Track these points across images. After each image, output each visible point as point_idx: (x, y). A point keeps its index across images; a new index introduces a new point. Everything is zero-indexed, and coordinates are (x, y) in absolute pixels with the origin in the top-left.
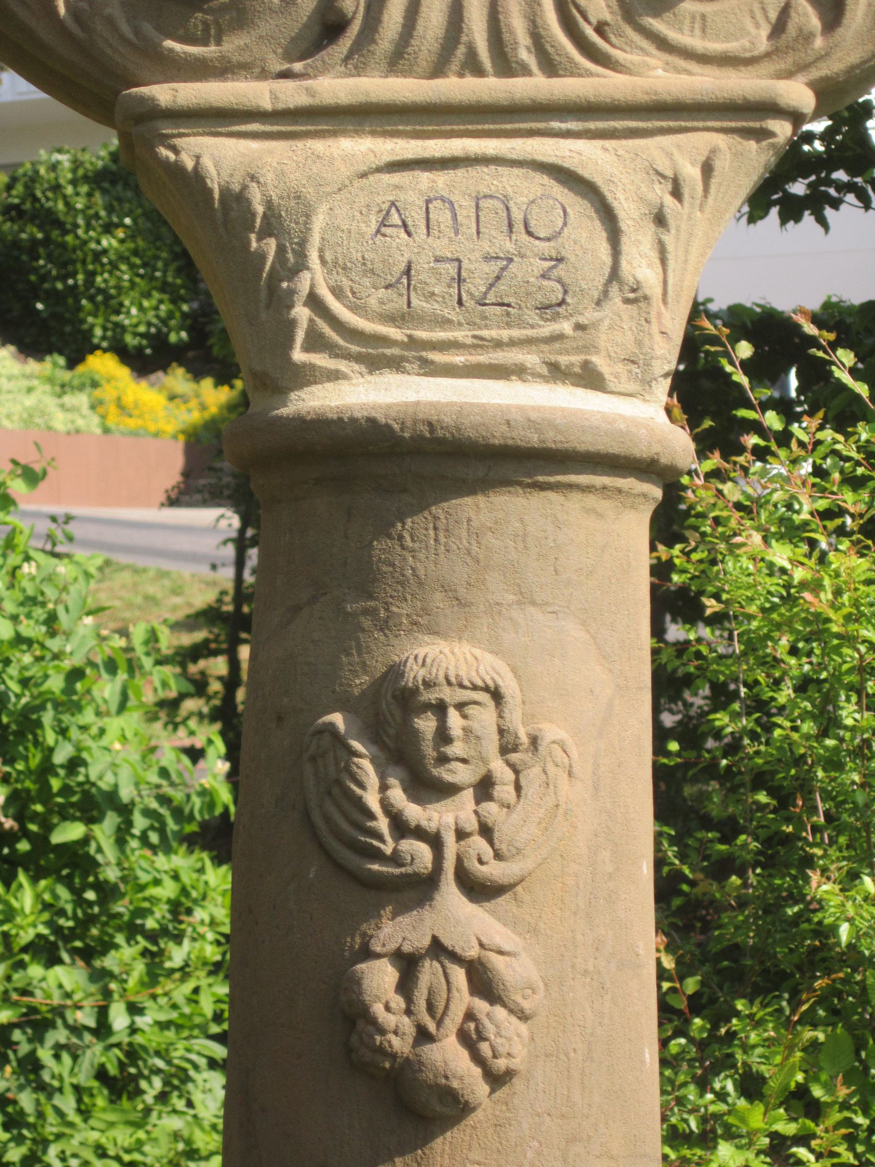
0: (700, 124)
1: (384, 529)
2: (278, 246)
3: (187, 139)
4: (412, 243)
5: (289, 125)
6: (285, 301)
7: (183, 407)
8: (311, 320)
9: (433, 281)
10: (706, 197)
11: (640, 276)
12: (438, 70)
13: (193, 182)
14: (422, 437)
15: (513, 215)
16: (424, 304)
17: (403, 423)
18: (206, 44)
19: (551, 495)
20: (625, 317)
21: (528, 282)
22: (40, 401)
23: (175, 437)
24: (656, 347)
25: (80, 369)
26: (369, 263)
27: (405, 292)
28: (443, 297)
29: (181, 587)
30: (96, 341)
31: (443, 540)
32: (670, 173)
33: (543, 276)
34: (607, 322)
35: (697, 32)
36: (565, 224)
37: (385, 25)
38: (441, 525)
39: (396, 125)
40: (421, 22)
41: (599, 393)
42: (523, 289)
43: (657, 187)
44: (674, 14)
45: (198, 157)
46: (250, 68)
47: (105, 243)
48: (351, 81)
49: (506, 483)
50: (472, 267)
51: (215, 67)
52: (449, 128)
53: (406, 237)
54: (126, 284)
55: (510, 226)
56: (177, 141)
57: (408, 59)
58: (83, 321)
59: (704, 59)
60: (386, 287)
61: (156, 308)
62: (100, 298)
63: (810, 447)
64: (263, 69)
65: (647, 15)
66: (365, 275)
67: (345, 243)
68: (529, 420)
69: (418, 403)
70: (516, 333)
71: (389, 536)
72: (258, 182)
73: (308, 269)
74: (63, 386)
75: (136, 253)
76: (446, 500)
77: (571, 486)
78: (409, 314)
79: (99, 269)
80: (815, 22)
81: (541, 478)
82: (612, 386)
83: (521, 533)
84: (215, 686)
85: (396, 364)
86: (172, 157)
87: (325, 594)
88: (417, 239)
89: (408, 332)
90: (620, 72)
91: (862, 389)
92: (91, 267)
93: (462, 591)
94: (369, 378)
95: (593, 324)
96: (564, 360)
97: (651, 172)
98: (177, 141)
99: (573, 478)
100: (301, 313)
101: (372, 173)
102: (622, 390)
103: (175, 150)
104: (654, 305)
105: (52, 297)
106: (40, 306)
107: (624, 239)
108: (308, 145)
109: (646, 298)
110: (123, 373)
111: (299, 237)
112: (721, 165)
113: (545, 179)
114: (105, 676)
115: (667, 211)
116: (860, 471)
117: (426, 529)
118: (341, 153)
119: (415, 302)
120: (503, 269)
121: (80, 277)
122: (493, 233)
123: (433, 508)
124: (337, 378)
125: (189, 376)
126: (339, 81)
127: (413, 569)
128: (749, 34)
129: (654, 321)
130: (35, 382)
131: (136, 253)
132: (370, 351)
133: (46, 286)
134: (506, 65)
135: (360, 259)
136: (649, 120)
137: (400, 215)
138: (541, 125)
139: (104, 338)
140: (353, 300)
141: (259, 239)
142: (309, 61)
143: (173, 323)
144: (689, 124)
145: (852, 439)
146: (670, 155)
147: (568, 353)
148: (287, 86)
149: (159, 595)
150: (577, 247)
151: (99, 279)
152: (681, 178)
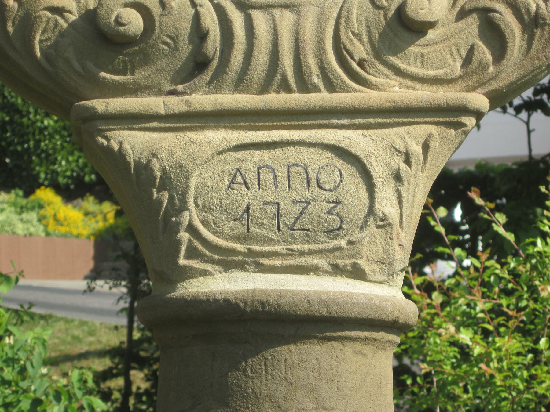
0: (422, 120)
1: (235, 365)
2: (169, 196)
3: (114, 132)
4: (249, 194)
5: (176, 123)
6: (175, 228)
7: (93, 220)
8: (190, 240)
9: (263, 216)
10: (425, 163)
11: (386, 212)
12: (264, 90)
13: (119, 157)
14: (257, 311)
15: (310, 176)
16: (257, 230)
17: (246, 303)
18: (125, 75)
19: (335, 344)
20: (377, 236)
21: (319, 216)
22: (8, 217)
23: (88, 237)
24: (396, 254)
25: (32, 197)
26: (224, 206)
27: (246, 223)
28: (269, 226)
29: (94, 331)
30: (41, 181)
31: (270, 371)
32: (403, 150)
33: (328, 213)
34: (367, 240)
35: (419, 64)
36: (341, 181)
37: (232, 63)
38: (269, 363)
39: (239, 123)
40: (254, 61)
41: (362, 282)
42: (316, 220)
43: (396, 158)
44: (405, 53)
45: (121, 143)
46: (151, 89)
47: (46, 123)
48: (212, 97)
49: (307, 337)
50: (286, 207)
51: (130, 88)
52: (271, 124)
53: (246, 190)
54: (59, 147)
55: (308, 183)
56: (109, 133)
57: (246, 83)
58: (34, 169)
59: (423, 80)
60: (235, 220)
61: (77, 161)
62: (43, 155)
63: (481, 270)
64: (159, 89)
65: (389, 55)
66: (221, 213)
67: (210, 194)
68: (321, 300)
69: (254, 290)
70: (312, 247)
71: (238, 370)
72: (157, 158)
73: (188, 209)
74: (22, 208)
75: (64, 128)
76: (272, 348)
77: (346, 338)
78: (248, 236)
79: (42, 138)
80: (489, 57)
81: (328, 334)
82: (370, 278)
83: (317, 367)
84: (116, 395)
85: (241, 266)
86: (106, 143)
87: (200, 404)
88: (253, 191)
89: (248, 247)
90: (373, 89)
91: (510, 237)
92: (37, 137)
93: (282, 403)
94: (224, 274)
95: (359, 241)
96: (341, 262)
97: (392, 149)
98: (109, 133)
99: (348, 333)
100: (184, 236)
101: (225, 152)
102: (376, 280)
103: (108, 139)
104: (395, 229)
105: (15, 155)
106: (8, 160)
107: (377, 190)
108: (187, 135)
109: (390, 225)
110: (57, 200)
111: (182, 191)
112: (434, 144)
113: (329, 154)
114: (54, 402)
115: (402, 172)
116: (510, 286)
117: (260, 365)
118: (206, 139)
119: (252, 229)
120: (304, 209)
121: (32, 143)
122: (298, 187)
123: (264, 353)
124: (206, 275)
125: (97, 201)
126: (205, 96)
127: (252, 389)
128: (450, 64)
129: (395, 238)
130: (5, 206)
131: (64, 128)
132: (225, 258)
133: (11, 148)
134: (305, 86)
135: (219, 203)
136: (390, 118)
137: (242, 177)
138: (326, 122)
139: (46, 179)
140: (214, 228)
141: (158, 192)
142: (187, 84)
143: (87, 170)
144: (415, 120)
145: (505, 267)
146: (403, 139)
147: (344, 258)
148: (174, 99)
149: (81, 336)
150: (349, 195)
151: (43, 144)
152: (410, 153)
